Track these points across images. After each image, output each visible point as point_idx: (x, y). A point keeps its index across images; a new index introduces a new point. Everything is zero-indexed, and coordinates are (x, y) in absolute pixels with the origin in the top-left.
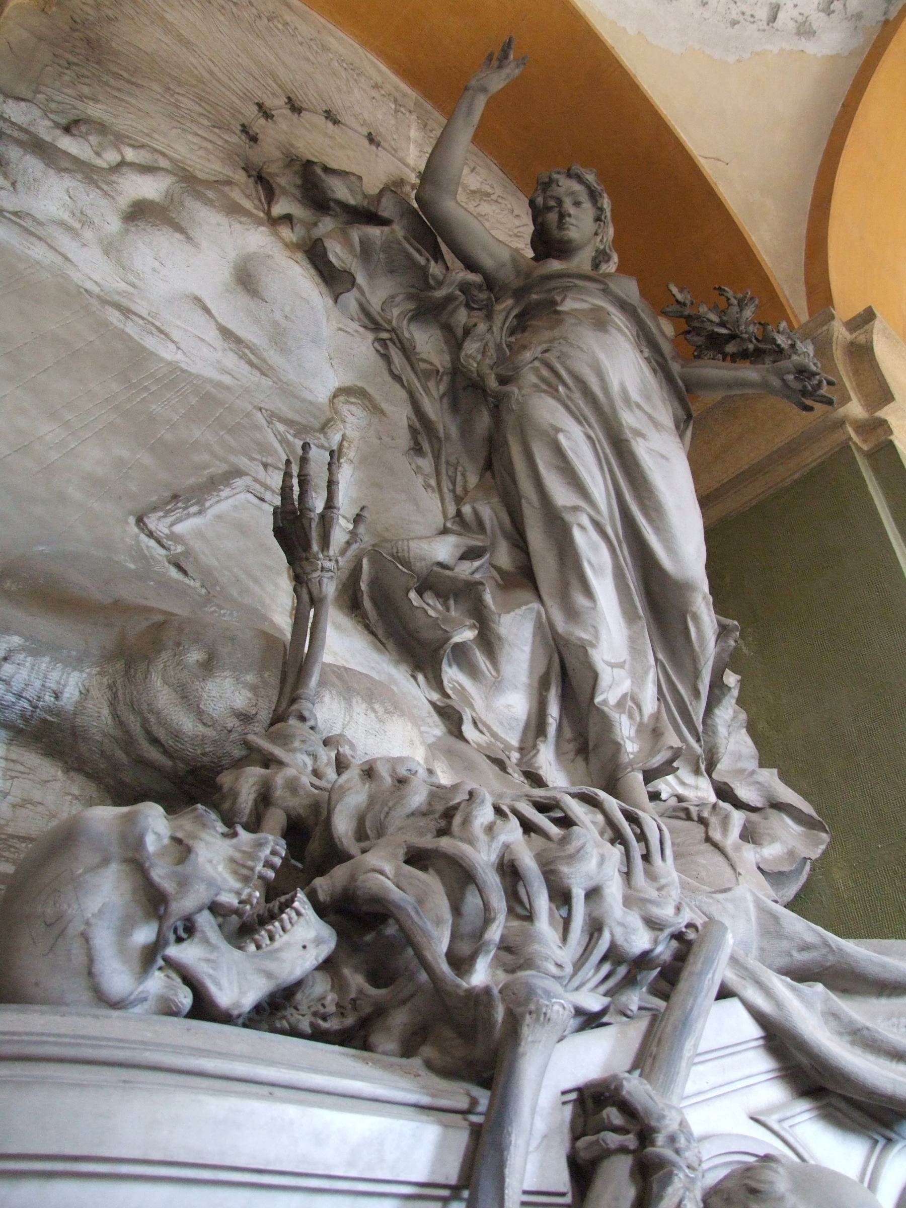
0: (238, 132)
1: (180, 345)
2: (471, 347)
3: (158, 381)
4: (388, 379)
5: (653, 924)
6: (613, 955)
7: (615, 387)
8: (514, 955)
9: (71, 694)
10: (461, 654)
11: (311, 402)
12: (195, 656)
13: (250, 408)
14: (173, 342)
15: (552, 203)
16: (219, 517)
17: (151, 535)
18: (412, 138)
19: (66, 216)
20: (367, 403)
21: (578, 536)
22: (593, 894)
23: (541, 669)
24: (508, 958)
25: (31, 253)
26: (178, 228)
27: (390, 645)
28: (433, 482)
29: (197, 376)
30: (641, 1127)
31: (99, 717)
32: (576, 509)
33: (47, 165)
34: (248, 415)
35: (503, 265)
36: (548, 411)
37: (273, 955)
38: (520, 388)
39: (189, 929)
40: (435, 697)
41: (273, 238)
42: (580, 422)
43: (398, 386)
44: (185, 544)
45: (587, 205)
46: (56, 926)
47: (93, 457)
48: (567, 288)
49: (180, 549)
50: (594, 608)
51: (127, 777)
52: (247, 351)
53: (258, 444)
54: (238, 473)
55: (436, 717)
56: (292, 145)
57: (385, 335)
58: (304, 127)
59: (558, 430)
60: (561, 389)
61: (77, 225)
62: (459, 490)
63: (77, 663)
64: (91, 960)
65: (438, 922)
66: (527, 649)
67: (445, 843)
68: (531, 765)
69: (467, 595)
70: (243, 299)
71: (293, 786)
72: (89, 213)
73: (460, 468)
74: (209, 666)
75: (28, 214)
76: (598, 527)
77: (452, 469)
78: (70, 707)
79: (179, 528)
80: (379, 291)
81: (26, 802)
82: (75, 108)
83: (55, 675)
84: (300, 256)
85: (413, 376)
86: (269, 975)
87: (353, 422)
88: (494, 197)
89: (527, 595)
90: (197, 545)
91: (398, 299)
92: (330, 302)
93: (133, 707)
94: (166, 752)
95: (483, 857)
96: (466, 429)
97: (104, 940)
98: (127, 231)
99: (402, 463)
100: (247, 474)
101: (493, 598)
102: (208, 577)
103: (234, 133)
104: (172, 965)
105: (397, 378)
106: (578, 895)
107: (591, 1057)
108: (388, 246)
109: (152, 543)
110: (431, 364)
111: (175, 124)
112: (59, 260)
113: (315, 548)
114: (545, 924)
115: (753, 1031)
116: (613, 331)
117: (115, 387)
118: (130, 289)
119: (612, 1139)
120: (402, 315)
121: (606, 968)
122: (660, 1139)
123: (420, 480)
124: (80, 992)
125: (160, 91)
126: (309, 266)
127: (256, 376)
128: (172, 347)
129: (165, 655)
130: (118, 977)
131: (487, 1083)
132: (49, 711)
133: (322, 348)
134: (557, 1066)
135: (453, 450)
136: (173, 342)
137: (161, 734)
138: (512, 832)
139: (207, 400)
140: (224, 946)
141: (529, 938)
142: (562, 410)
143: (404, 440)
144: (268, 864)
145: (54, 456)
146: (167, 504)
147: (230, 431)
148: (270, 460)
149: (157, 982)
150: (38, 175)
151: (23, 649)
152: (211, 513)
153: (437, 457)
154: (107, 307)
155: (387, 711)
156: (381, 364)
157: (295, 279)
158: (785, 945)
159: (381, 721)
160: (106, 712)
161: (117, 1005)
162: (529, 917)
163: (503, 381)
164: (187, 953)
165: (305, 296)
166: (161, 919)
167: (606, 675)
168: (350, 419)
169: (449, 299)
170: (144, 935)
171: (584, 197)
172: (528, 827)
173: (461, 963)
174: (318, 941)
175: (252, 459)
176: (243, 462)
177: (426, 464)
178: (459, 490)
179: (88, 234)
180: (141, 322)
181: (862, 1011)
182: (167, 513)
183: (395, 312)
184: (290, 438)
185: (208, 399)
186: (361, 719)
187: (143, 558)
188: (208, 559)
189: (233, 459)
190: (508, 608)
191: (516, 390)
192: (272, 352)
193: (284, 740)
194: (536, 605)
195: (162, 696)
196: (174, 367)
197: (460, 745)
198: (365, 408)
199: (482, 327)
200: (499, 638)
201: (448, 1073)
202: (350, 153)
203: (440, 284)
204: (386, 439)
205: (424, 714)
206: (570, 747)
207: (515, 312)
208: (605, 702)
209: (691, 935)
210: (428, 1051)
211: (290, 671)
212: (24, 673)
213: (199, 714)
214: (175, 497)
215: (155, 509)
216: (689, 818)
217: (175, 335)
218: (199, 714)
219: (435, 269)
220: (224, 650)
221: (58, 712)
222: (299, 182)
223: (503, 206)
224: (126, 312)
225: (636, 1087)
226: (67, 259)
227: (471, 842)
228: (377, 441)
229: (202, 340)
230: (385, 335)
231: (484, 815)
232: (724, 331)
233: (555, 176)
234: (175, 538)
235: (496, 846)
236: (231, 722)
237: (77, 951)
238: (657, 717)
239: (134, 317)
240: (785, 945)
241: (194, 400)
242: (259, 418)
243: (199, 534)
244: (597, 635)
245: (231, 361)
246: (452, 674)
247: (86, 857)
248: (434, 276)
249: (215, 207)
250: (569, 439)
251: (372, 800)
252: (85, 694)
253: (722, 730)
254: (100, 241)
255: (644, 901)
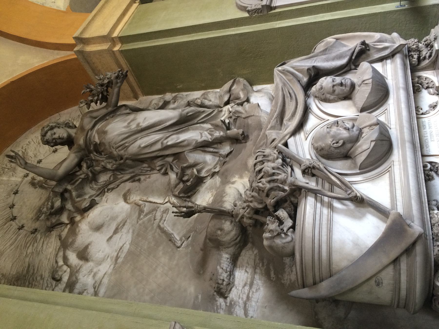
0: (35, 235)
1: (124, 243)
2: (109, 166)
3: (137, 248)
4: (118, 188)
5: (277, 158)
6: (282, 165)
7: (124, 130)
8: (284, 182)
9: (227, 256)
10: (199, 171)
11: (131, 209)
12: (219, 232)
13: (138, 225)
14: (123, 245)
15: (54, 141)
16: (173, 230)
17: (182, 245)
18: (7, 179)
19: (91, 276)
20: (128, 194)
21: (169, 143)
22: (273, 169)
23: (201, 152)
24: (283, 183)
25: (106, 282)
26: (87, 247)
27: (198, 188)
28: (148, 176)
29: (132, 238)
30: (308, 168)
31: (231, 250)
32: (162, 143)
33: (77, 282)
34: (140, 225)
35: (76, 156)
36: (133, 148)
37: (285, 218)
38: (125, 155)
39: (282, 230)
40: (209, 178)
41: (82, 222)
42: (137, 140)
43: (120, 186)
44: (182, 237)
45: (55, 130)
46: (283, 247)
47: (164, 260)
48: (90, 140)
49: (183, 238)
50: (188, 140)
51: (242, 244)
52: (120, 227)
53: (148, 222)
54: (159, 226)
55: (214, 177)
56: (32, 218)
57: (106, 190)
58: (21, 215)
59: (140, 147)
60: (127, 145)
61: (93, 273)
62: (149, 169)
63: (221, 256)
64: (287, 242)
65: (279, 193)
66: (195, 155)
67: (266, 191)
68: (225, 156)
69: (183, 170)
70: (104, 229)
71: (248, 213)
72: (88, 271)
73: (142, 169)
74: (221, 229)
75: (94, 285)
76: (167, 138)
77: (143, 171)
78: (230, 256)
79: (178, 239)
80: (90, 191)
81: (248, 263)
82: (48, 280)
83: (224, 259)
84: (86, 214)
85: (117, 182)
86: (287, 218)
87: (135, 198)
88: (24, 151)
89: (182, 155)
90: (181, 234)
91: (91, 186)
92: (98, 205)
93: (229, 243)
94: (238, 237)
95: (268, 186)
96: (131, 167)
97: (284, 241)
98: (92, 260)
99: (143, 184)
100: (159, 224)
101: (185, 164)
102: (189, 231)
103: (36, 236)
104: (287, 232)
105: (118, 186)
106: (274, 171)
107: (298, 172)
108: (76, 189)
109: (183, 244)
110: (111, 176)
111: (41, 253)
112: (106, 276)
113: (193, 209)
114: (279, 177)
115: (292, 138)
116: (107, 129)
117: (142, 257)
118: (109, 257)
119: (310, 172)
120: (96, 185)
121: (284, 166)
122: (310, 166)
123: (148, 180)
124: (292, 244)
125: (28, 259)
126: (89, 212)
127: (127, 223)
128: (125, 245)
129: (219, 238)
130: (289, 239)
131: (302, 189)
132: (231, 260)
133: (113, 207)
134: (300, 178)
135: (137, 171)
136: (123, 245)
137: (235, 238)
138: (263, 180)
139: (138, 236)
140: (284, 225)
141: (281, 180)
142: (133, 145)
143: (136, 184)
144: (272, 219)
145: (166, 268)
146: (172, 242)
147: (147, 229)
148: (153, 219)
149: (289, 234)
150: (81, 284)
151: (220, 266)
152: (172, 232)
153: (140, 175)
154: (118, 262)
155: (225, 193)
156: (114, 190)
157: (94, 215)
158: (276, 125)
159: (227, 194)
160: (230, 249)
161: (292, 238)
162: (278, 179)
163: (122, 159)
164: (285, 230)
165: (99, 212)
166: (281, 233)
167: (204, 138)
168: (134, 198)
169: (91, 172)
170: (283, 235)
171: (52, 132)
172: (262, 177)
173: (284, 190)
174: (282, 211)
175: (154, 223)
176: (155, 225)
177: (142, 178)
178: (149, 169)
179: (95, 270)
180: (120, 254)
181: (288, 115)
182: (175, 242)
183: (95, 186)
184: (144, 214)
185: (138, 235)
186: (227, 198)
187: (187, 246)
188: (185, 231)
189: (155, 228)
190: (187, 160)
191: (126, 156)
192: (118, 220)
193: (237, 215)
194: (185, 153)
195: (227, 238)
196: (131, 244)
197: (220, 172)
198: (130, 195)
199: (103, 164)
200: (194, 162)
201: (300, 194)
202: (26, 200)
203: (87, 175)
204: (137, 189)
205: (213, 180)
206: (219, 145)
207: (95, 154)
208: (211, 139)
209: (279, 151)
210: (297, 196)
211: (218, 213)
212: (225, 265)
213: (231, 231)
214: (170, 240)
215: (175, 244)
216: (237, 119)
217: (121, 245)
218: (231, 231)
219: (83, 176)
220: (217, 227)
221: (231, 258)
222: (54, 216)
223: (26, 147)
224: (117, 258)
225: (303, 167)
226: (105, 274)
227: (265, 188)
228: (139, 191)
229: (120, 238)
230: (106, 190)
231: (260, 184)
232: (101, 95)
233: (45, 140)
234: (181, 239)
235: (266, 184)
236: (233, 224)
237: (286, 244)
238: (212, 125)
239: (119, 255)
240: (276, 125)
241: (140, 239)
242: (140, 222)
243: (178, 234)
244: (195, 140)
245: (124, 230)
246: (203, 174)
247: (273, 244)
248: (85, 176)
249: (75, 239)
250: (142, 144)
251: (256, 201)
252: (227, 253)
253: (211, 103)
254: (97, 267)
255: (274, 159)
